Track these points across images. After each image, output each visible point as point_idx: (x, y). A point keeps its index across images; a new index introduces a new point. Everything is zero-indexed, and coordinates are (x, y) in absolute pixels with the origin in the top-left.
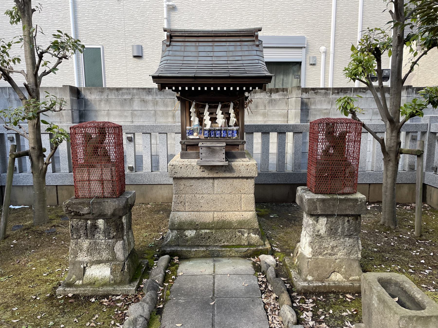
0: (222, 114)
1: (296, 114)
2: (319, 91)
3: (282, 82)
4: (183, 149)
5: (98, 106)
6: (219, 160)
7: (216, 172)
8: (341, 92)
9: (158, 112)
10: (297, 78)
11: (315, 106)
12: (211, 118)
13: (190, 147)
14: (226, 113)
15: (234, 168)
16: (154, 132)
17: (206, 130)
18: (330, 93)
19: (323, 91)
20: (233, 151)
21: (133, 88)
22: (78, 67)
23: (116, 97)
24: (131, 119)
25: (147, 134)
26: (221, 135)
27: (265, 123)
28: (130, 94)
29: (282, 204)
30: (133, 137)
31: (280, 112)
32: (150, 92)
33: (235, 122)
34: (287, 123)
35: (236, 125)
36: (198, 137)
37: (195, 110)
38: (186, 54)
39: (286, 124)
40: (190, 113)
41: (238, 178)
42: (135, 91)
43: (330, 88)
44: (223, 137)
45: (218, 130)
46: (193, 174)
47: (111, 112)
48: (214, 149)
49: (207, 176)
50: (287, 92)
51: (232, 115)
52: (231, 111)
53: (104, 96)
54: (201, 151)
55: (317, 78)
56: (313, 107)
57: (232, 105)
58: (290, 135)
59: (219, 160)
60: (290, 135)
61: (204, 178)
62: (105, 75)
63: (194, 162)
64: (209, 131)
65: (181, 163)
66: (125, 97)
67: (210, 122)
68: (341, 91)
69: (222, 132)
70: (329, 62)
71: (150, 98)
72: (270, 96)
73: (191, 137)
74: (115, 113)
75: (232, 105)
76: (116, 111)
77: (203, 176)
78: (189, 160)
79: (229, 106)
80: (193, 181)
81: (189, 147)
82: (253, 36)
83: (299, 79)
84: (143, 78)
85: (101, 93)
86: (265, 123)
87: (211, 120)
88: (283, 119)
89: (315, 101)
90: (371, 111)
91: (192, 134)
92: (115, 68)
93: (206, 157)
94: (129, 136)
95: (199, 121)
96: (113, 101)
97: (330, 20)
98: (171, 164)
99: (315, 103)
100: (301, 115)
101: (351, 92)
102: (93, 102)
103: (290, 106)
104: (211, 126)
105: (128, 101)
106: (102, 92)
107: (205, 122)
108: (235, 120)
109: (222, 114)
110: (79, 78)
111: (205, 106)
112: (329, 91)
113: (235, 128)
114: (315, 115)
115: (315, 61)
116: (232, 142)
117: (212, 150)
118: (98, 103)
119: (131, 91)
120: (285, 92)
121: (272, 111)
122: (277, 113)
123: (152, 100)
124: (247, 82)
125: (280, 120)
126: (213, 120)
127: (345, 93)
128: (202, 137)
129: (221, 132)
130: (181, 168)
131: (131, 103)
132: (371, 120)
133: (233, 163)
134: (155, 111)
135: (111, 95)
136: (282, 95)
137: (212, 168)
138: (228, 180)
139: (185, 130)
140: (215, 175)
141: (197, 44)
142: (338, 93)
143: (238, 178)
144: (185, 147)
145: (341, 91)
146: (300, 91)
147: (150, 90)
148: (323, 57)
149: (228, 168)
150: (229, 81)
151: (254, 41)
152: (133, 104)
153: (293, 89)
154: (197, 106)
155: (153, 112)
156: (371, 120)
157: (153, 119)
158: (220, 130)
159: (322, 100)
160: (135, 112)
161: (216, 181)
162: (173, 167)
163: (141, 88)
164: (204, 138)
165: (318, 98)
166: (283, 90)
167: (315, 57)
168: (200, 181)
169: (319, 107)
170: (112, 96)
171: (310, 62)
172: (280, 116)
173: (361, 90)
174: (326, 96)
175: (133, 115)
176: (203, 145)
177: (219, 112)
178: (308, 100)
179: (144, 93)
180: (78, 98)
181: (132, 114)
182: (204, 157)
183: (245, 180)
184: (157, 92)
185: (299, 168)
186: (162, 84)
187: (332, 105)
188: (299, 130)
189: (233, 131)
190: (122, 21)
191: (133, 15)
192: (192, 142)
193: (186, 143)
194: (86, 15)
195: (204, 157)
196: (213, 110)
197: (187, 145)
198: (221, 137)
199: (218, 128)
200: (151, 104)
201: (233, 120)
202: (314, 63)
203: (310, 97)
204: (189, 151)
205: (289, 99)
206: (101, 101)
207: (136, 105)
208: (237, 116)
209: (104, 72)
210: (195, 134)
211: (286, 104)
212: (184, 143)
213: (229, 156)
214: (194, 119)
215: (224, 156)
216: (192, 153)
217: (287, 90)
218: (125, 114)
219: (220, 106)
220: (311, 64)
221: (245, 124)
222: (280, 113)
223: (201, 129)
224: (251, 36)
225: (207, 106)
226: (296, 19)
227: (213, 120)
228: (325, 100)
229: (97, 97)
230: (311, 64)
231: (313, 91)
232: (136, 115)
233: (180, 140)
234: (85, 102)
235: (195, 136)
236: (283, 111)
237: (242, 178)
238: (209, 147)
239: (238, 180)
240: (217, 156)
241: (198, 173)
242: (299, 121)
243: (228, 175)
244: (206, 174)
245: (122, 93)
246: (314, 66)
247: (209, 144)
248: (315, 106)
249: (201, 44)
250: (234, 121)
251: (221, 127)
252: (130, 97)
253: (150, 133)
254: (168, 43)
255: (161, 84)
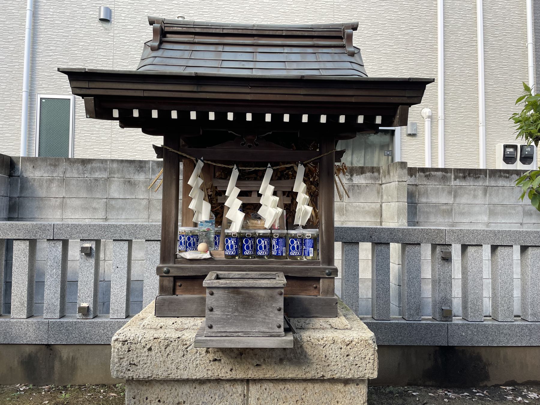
0: (275, 194)
1: (399, 210)
2: (432, 173)
3: (363, 161)
4: (163, 289)
5: (44, 191)
6: (265, 332)
7: (255, 362)
8: (470, 176)
9: (155, 202)
10: (388, 155)
11: (427, 198)
12: (243, 204)
13: (184, 284)
14: (284, 193)
15: (309, 351)
16: (136, 238)
17: (229, 236)
18: (451, 177)
19: (439, 174)
20: (303, 296)
21: (113, 161)
22: (30, 128)
23: (80, 174)
24: (104, 213)
25: (122, 243)
26: (270, 249)
27: (342, 224)
28: (105, 170)
29: (388, 390)
30: (94, 247)
31: (367, 207)
32: (141, 167)
33: (308, 217)
34: (381, 225)
35: (310, 225)
36: (207, 256)
37: (201, 181)
38: (191, 63)
39: (378, 227)
40: (188, 188)
41: (322, 380)
42: (115, 165)
43: (451, 169)
44: (277, 257)
45: (264, 237)
46: (185, 368)
47: (68, 201)
48: (251, 297)
49: (228, 377)
50: (379, 174)
51: (302, 197)
52: (300, 187)
53: (59, 173)
54: (210, 301)
55: (419, 157)
56: (424, 200)
57: (301, 171)
58: (395, 248)
59: (265, 332)
60: (395, 248)
61: (218, 381)
62: (73, 141)
63: (189, 328)
64: (240, 238)
65: (150, 335)
66: (97, 175)
67: (242, 215)
68: (469, 174)
69: (274, 242)
70: (437, 131)
71: (141, 177)
72: (351, 179)
73: (189, 255)
74: (77, 202)
75: (301, 171)
76: (77, 200)
77: (215, 377)
78: (179, 320)
79: (294, 177)
80: (186, 389)
81: (180, 284)
82: (341, 38)
83: (390, 158)
84: (138, 148)
85: (52, 168)
86: (342, 224)
87: (244, 208)
88: (373, 220)
89: (427, 190)
90: (520, 209)
91: (194, 247)
92: (93, 131)
93: (225, 321)
94: (87, 245)
95: (212, 210)
96: (74, 182)
97: (435, 70)
98: (122, 338)
99: (426, 193)
100: (408, 212)
101: (486, 176)
102: (36, 184)
103: (385, 197)
104: (243, 227)
105: (101, 182)
106: (55, 166)
107: (229, 215)
108: (310, 209)
109: (275, 194)
110: (29, 146)
111: (230, 172)
112: (449, 174)
113: (309, 233)
114: (427, 213)
115: (416, 130)
116: (301, 270)
117: (244, 300)
118: (45, 185)
119: (109, 165)
120: (376, 174)
121: (354, 204)
122: (363, 208)
123: (145, 182)
124: (353, 100)
125: (368, 219)
126: (251, 209)
127: (476, 178)
128: (220, 254)
129: (270, 244)
130: (150, 349)
131: (106, 185)
132: (521, 224)
133: (305, 335)
134: (149, 201)
135: (72, 172)
136: (371, 178)
137: (241, 355)
138: (288, 386)
139: (172, 235)
140: (252, 374)
141: (220, 48)
142: (464, 177)
143: (322, 380)
144: (168, 282)
145: (469, 174)
146: (406, 171)
147: (142, 165)
148: (427, 123)
149: (295, 355)
150: (300, 95)
151: (343, 47)
152: (110, 188)
153: (391, 168)
154: (207, 172)
155: (144, 202)
156: (521, 224)
157: (145, 215)
158: (269, 237)
159: (438, 188)
160: (113, 202)
161: (254, 389)
162: (126, 347)
163: (127, 161)
164: (223, 257)
165: (431, 185)
166: (373, 170)
167: (416, 123)
168: (206, 387)
169: (433, 200)
170: (73, 173)
171: (407, 131)
172: (368, 213)
173: (502, 174)
174: (444, 182)
175: (108, 207)
176: (217, 283)
177: (267, 189)
178: (414, 188)
179: (132, 169)
180: (10, 176)
181: (106, 204)
182: (218, 321)
183: (340, 387)
184: (155, 167)
185: (418, 314)
186: (97, 98)
187: (455, 197)
188: (414, 240)
189: (302, 240)
190: (109, 59)
191: (128, 51)
192: (191, 270)
193: (174, 273)
194: (51, 48)
195: (218, 321)
196: (250, 185)
197: (176, 279)
198: (270, 256)
199: (262, 232)
200: (143, 189)
201: (304, 209)
202: (413, 132)
203: (417, 182)
204: (182, 296)
205: (383, 186)
206: (51, 181)
207: (116, 191)
208: (313, 201)
209: (74, 138)
210: (202, 246)
211: (378, 193)
212: (168, 272)
213: (295, 313)
214: (199, 206)
215: (280, 318)
216: (188, 300)
217: (378, 170)
218: (95, 205)
219: (269, 173)
220: (410, 135)
221: (337, 224)
222: (367, 208)
223: (218, 235)
224: (337, 37)
225: (235, 174)
226: (383, 68)
227: (251, 209)
228: (442, 188)
229: (46, 175)
230: (410, 135)
231: (422, 174)
232: (113, 208)
233: (158, 263)
234: (22, 183)
235: (201, 252)
236: (373, 205)
237: (333, 381)
238: (235, 290)
239: (318, 387)
240: (260, 316)
241: (200, 366)
242: (405, 222)
243: (290, 372)
244: (223, 371)
245: (92, 169)
246: (414, 138)
247: (235, 279)
248: (427, 198)
249: (227, 48)
250: (306, 212)
251: (271, 229)
252: (105, 175)
253: (130, 242)
254: (156, 44)
255: (96, 97)
